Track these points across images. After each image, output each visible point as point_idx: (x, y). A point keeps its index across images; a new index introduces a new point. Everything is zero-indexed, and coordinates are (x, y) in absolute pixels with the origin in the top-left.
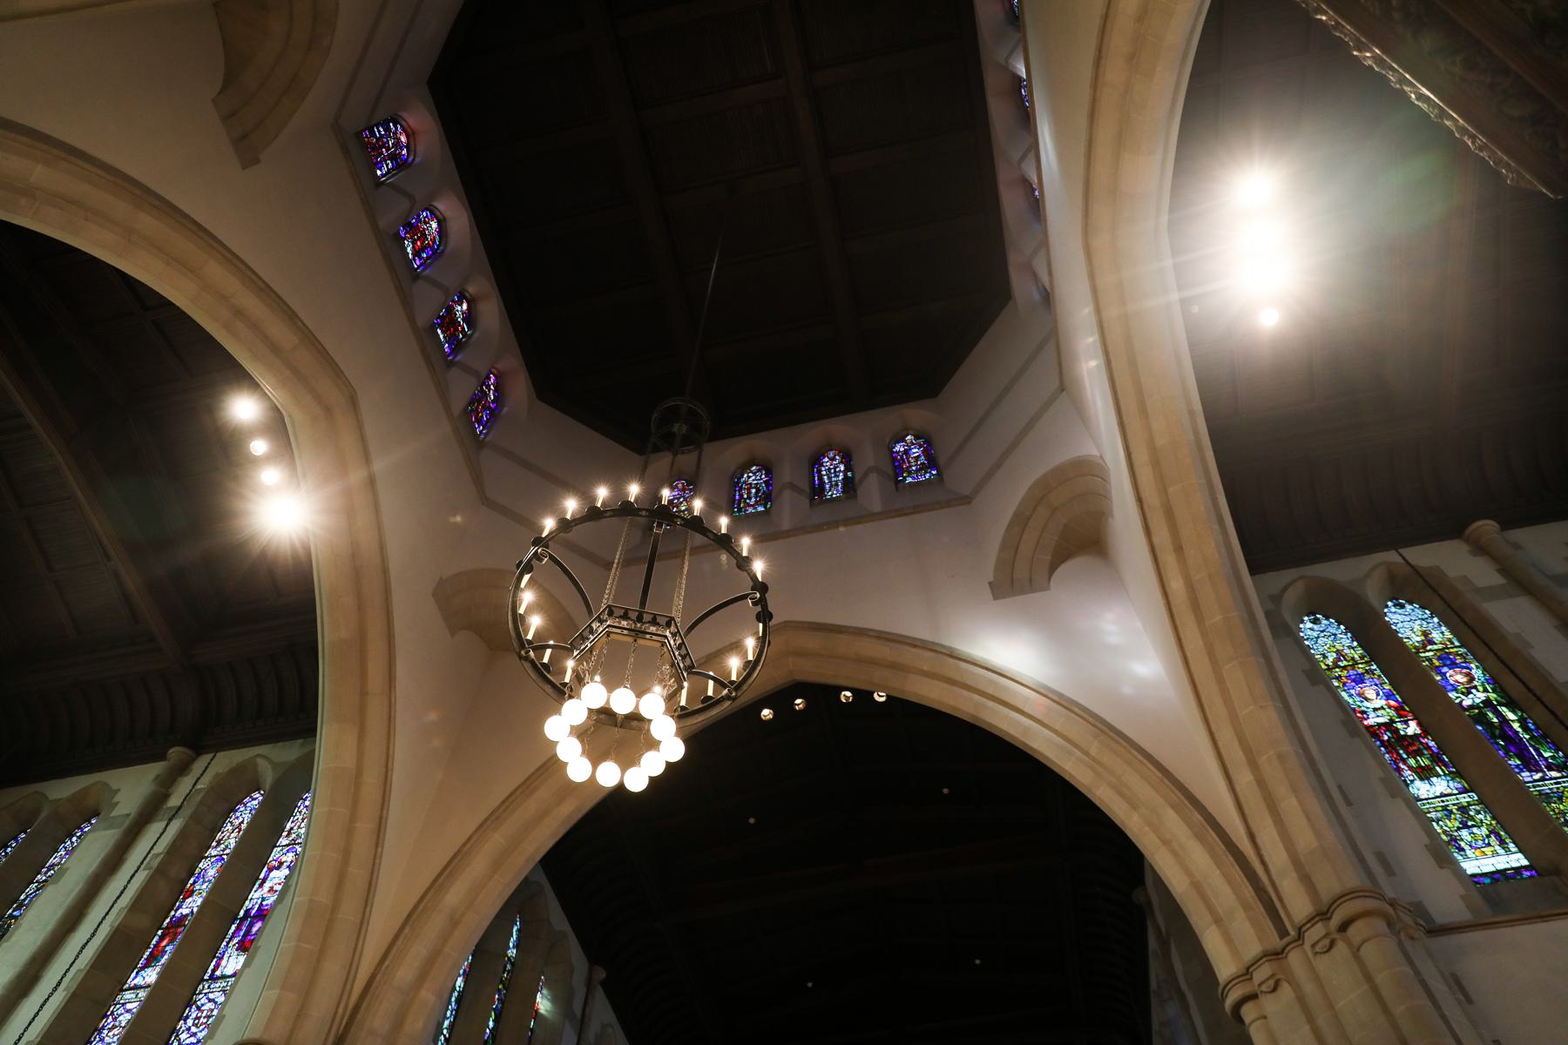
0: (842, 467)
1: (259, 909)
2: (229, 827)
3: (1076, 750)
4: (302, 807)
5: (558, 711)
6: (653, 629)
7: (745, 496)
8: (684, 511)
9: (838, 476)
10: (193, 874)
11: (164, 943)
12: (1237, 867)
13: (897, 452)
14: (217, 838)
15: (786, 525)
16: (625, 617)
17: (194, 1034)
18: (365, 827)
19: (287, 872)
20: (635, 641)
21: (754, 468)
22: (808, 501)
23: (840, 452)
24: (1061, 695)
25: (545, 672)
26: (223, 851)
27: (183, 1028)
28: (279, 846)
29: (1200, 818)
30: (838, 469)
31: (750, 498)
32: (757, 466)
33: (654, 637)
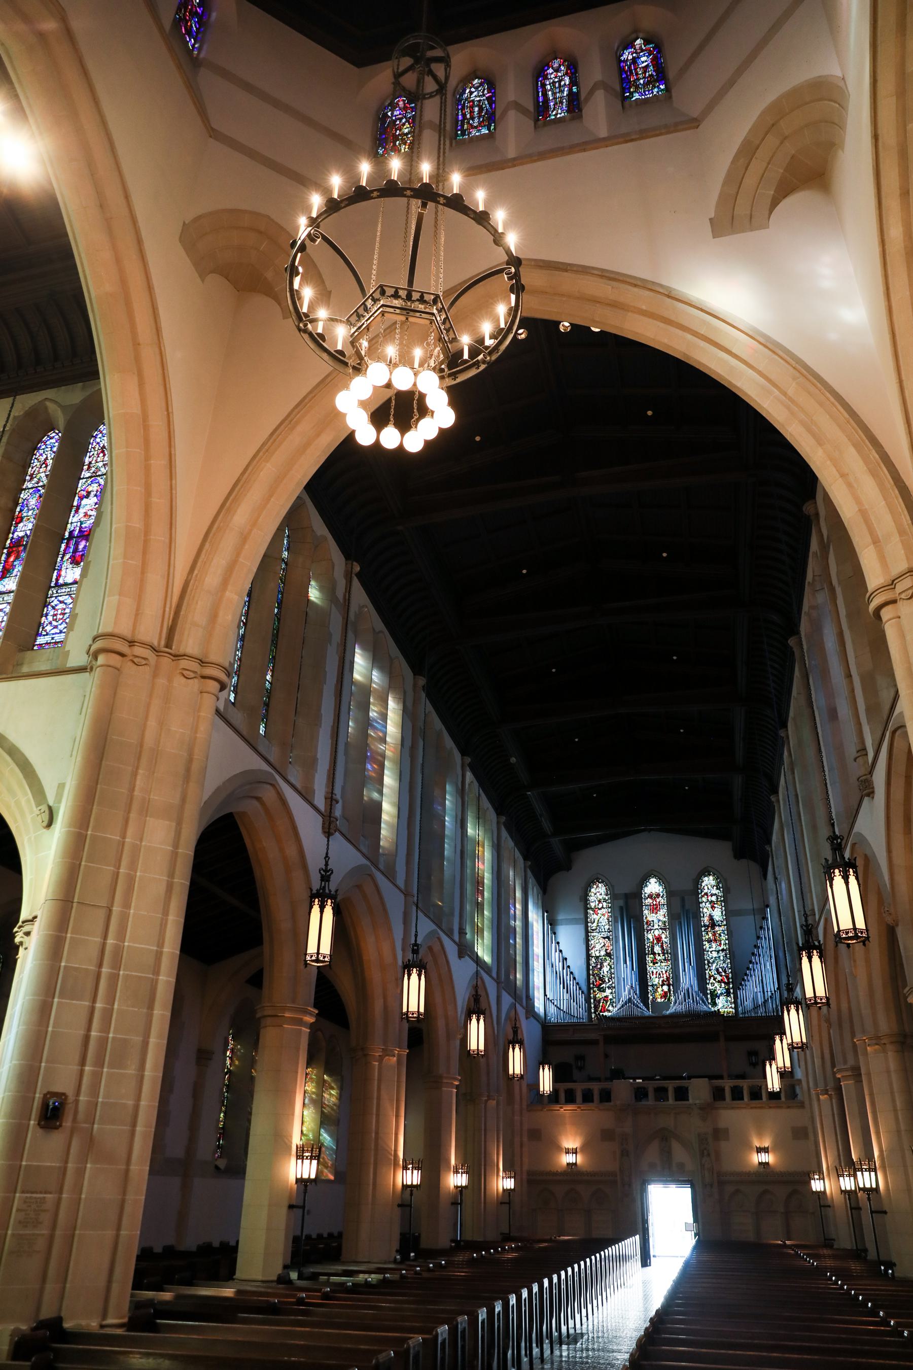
0: (567, 80)
1: (80, 531)
2: (36, 463)
3: (776, 390)
4: (94, 444)
5: (346, 386)
6: (421, 307)
7: (468, 116)
8: (407, 134)
9: (563, 92)
10: (17, 504)
11: (12, 559)
12: (900, 500)
13: (626, 61)
14: (29, 473)
15: (511, 153)
16: (396, 296)
17: (56, 627)
18: (158, 463)
19: (95, 500)
20: (407, 319)
21: (476, 81)
22: (532, 123)
23: (565, 61)
24: (768, 338)
25: (321, 341)
26: (37, 483)
27: (46, 622)
28: (83, 478)
29: (877, 456)
30: (563, 83)
31: (472, 118)
32: (479, 78)
33: (424, 315)
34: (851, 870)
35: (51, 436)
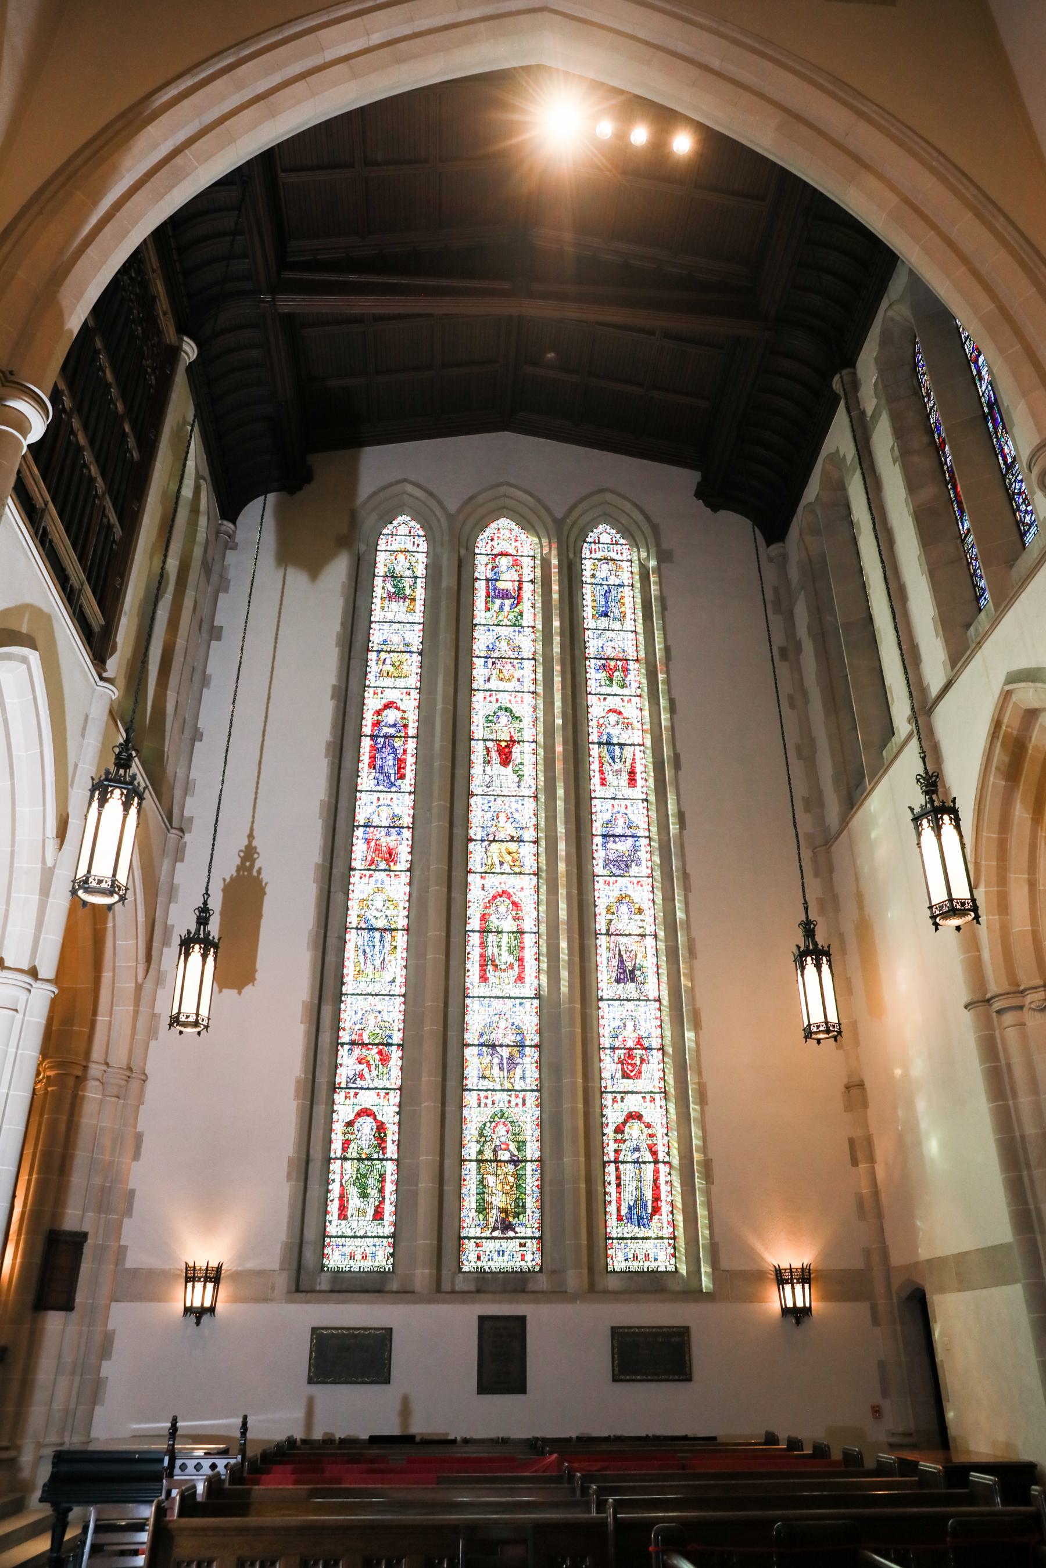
34: (824, 958)
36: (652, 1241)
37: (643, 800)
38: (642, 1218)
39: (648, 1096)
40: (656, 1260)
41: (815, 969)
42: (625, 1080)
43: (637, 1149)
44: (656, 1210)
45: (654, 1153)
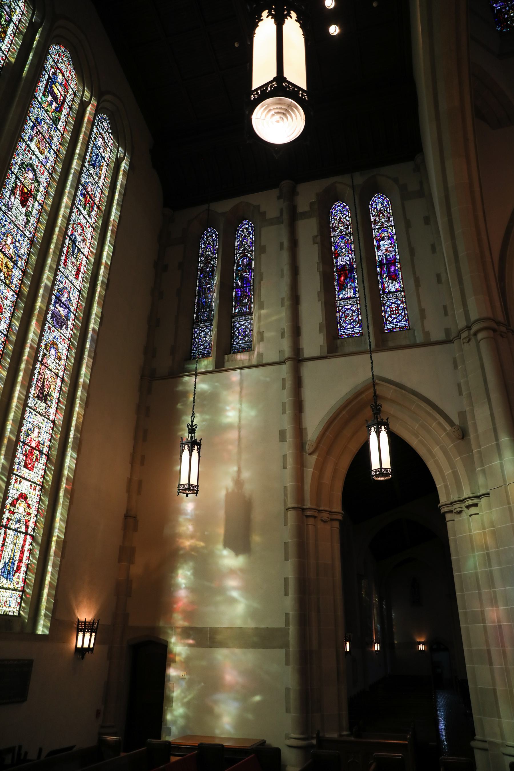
35: (338, 205)
36: (10, 591)
37: (79, 292)
38: (10, 574)
39: (33, 485)
40: (10, 606)
41: (188, 452)
42: (25, 469)
43: (19, 521)
44: (19, 568)
45: (27, 527)
